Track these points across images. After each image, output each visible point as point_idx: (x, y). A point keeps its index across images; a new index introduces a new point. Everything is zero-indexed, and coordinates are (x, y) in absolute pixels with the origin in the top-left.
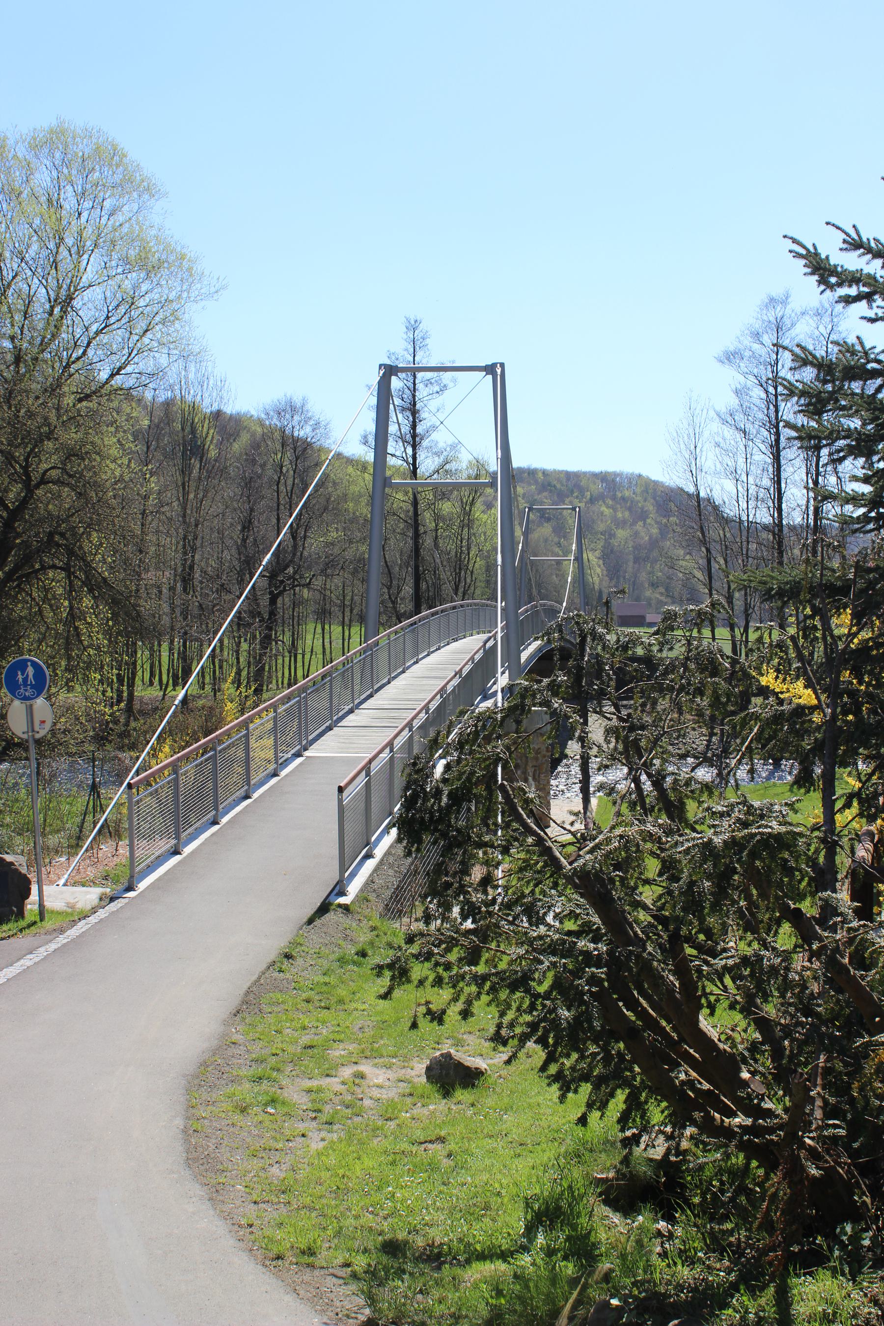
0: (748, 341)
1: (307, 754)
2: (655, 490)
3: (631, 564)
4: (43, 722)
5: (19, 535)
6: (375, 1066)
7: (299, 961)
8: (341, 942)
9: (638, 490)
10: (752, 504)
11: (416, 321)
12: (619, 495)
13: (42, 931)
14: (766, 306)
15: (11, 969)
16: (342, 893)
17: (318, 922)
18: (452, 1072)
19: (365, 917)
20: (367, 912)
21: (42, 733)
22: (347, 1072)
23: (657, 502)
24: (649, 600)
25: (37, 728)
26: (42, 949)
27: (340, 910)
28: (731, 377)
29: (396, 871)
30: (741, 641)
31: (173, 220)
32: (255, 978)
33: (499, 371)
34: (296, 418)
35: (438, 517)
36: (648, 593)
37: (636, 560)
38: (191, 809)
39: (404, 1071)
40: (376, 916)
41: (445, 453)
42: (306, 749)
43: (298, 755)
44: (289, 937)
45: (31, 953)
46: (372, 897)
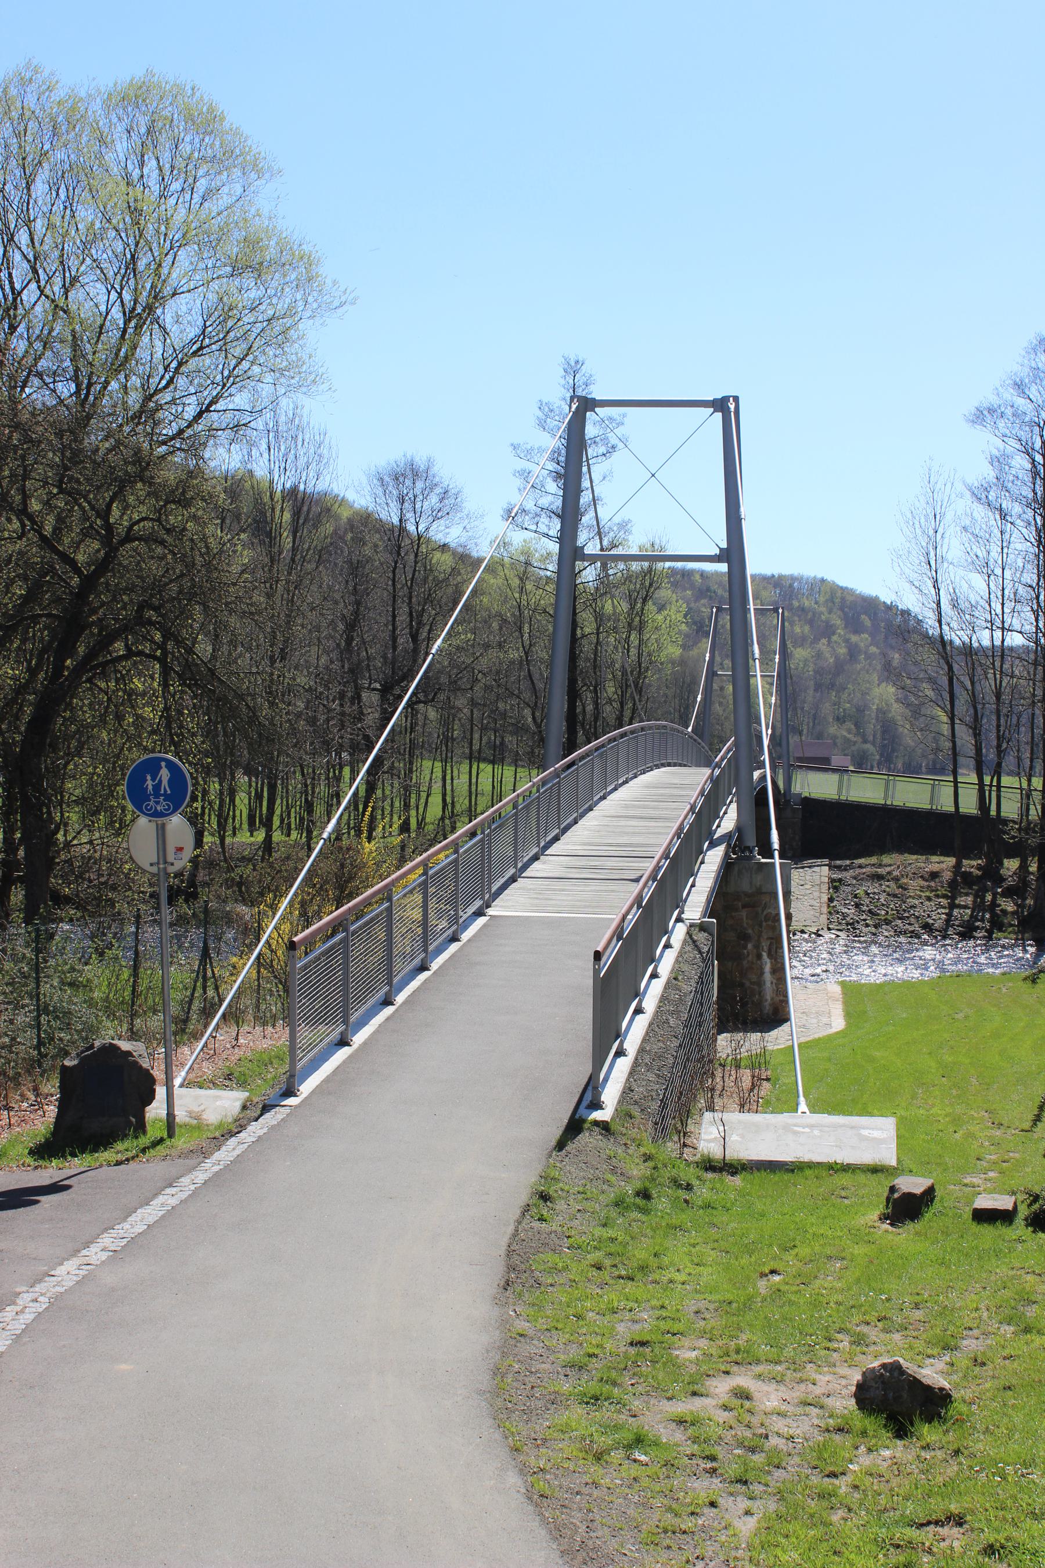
0: (1010, 395)
1: (490, 912)
2: (843, 599)
3: (811, 692)
4: (181, 849)
5: (94, 611)
6: (759, 1377)
7: (560, 1205)
8: (609, 1176)
9: (822, 599)
10: (1009, 606)
11: (577, 362)
12: (796, 604)
13: (174, 1152)
14: (1034, 349)
15: (147, 1210)
16: (597, 1105)
17: (570, 1147)
18: (905, 1395)
19: (633, 1140)
20: (634, 1133)
21: (178, 866)
22: (721, 1387)
23: (845, 614)
24: (834, 738)
25: (170, 858)
26: (185, 1180)
27: (596, 1129)
28: (985, 442)
29: (658, 1076)
30: (991, 786)
31: (289, 206)
32: (510, 1229)
33: (732, 407)
34: (420, 485)
35: (599, 617)
36: (833, 730)
37: (818, 687)
38: (334, 985)
39: (802, 1386)
40: (646, 1137)
41: (612, 534)
42: (488, 906)
43: (479, 913)
44: (538, 1168)
45: (171, 1185)
46: (635, 1111)
